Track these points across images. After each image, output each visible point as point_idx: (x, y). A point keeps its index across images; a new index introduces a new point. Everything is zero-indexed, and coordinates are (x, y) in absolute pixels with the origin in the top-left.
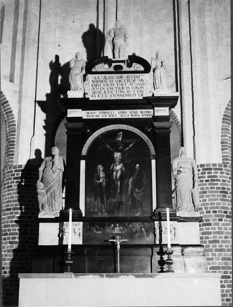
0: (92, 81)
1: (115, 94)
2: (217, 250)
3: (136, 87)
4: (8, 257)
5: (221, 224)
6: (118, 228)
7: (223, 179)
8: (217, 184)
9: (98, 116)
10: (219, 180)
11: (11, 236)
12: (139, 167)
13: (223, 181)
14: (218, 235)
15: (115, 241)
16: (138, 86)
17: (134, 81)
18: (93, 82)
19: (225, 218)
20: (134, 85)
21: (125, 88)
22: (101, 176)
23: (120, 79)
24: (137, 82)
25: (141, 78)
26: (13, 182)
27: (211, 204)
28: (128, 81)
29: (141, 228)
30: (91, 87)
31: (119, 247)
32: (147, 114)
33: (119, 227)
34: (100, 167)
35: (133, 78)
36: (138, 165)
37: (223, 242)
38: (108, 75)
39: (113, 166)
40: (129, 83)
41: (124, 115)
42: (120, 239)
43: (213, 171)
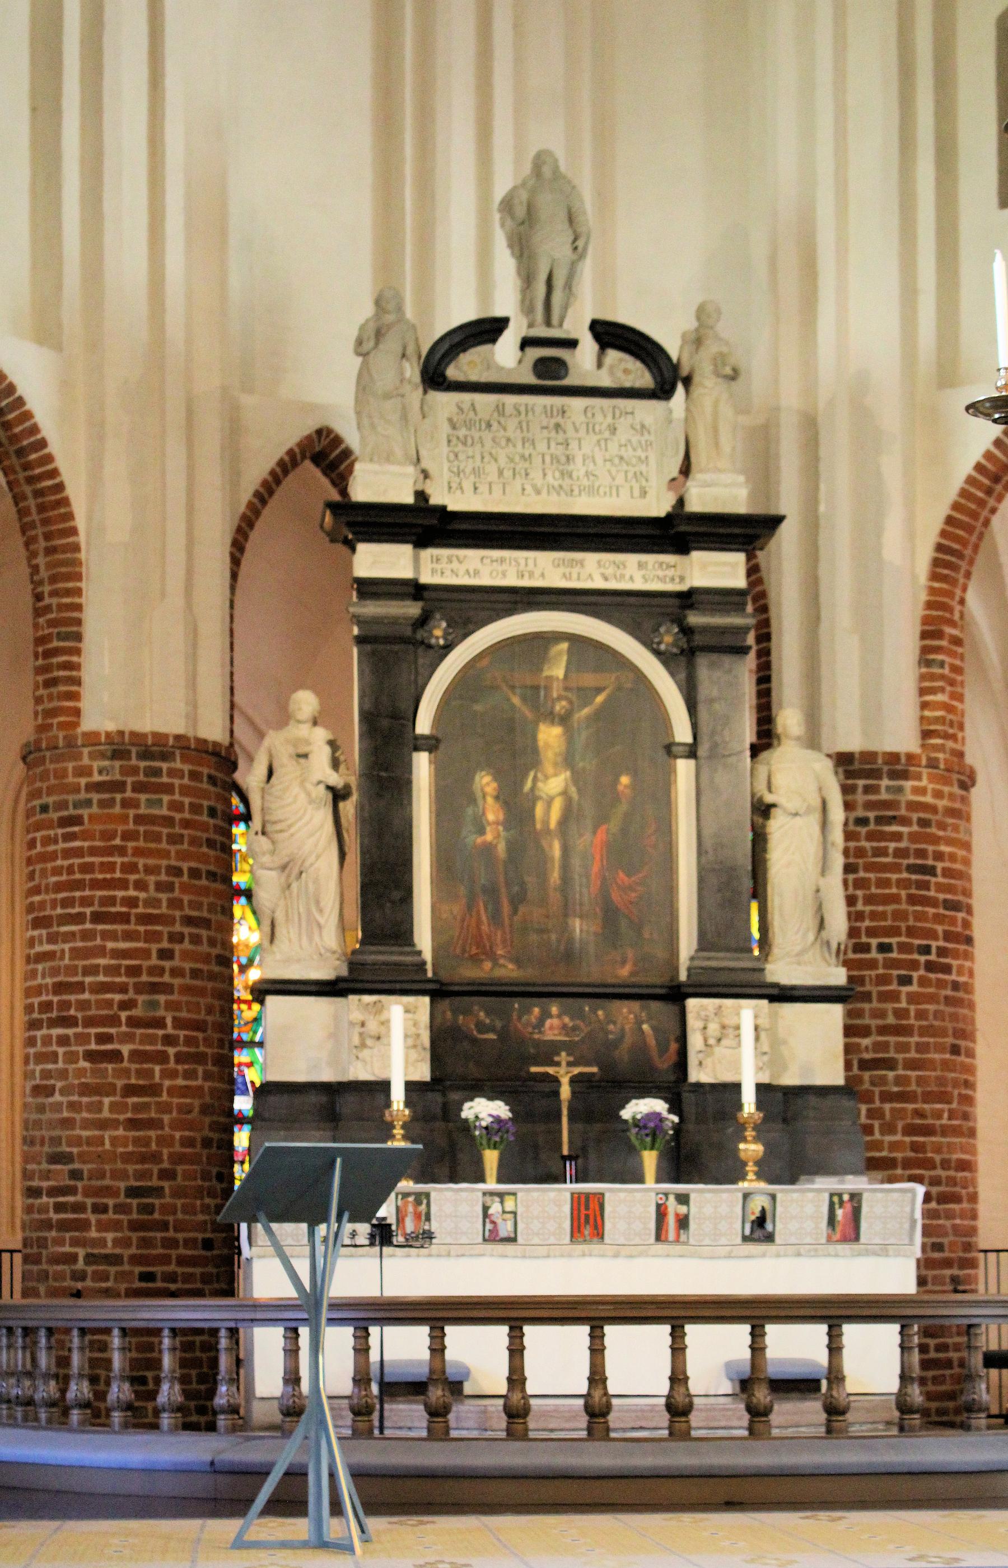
0: (450, 420)
1: (539, 482)
2: (887, 1097)
3: (621, 458)
4: (85, 1115)
5: (909, 994)
6: (555, 1022)
7: (922, 815)
8: (897, 837)
9: (477, 573)
10: (905, 821)
11: (93, 1031)
12: (633, 786)
13: (924, 823)
14: (892, 1039)
15: (551, 1070)
16: (628, 453)
17: (613, 430)
18: (454, 427)
19: (922, 972)
20: (613, 448)
21: (579, 460)
22: (491, 817)
23: (559, 419)
24: (624, 434)
25: (638, 419)
26: (88, 803)
27: (874, 916)
28: (590, 428)
29: (639, 1023)
30: (445, 449)
31: (565, 1092)
32: (660, 573)
33: (559, 1016)
34: (485, 782)
35: (609, 419)
36: (625, 780)
37: (912, 1065)
38: (510, 400)
39: (535, 779)
40: (596, 438)
41: (575, 571)
42: (569, 1064)
43: (885, 782)
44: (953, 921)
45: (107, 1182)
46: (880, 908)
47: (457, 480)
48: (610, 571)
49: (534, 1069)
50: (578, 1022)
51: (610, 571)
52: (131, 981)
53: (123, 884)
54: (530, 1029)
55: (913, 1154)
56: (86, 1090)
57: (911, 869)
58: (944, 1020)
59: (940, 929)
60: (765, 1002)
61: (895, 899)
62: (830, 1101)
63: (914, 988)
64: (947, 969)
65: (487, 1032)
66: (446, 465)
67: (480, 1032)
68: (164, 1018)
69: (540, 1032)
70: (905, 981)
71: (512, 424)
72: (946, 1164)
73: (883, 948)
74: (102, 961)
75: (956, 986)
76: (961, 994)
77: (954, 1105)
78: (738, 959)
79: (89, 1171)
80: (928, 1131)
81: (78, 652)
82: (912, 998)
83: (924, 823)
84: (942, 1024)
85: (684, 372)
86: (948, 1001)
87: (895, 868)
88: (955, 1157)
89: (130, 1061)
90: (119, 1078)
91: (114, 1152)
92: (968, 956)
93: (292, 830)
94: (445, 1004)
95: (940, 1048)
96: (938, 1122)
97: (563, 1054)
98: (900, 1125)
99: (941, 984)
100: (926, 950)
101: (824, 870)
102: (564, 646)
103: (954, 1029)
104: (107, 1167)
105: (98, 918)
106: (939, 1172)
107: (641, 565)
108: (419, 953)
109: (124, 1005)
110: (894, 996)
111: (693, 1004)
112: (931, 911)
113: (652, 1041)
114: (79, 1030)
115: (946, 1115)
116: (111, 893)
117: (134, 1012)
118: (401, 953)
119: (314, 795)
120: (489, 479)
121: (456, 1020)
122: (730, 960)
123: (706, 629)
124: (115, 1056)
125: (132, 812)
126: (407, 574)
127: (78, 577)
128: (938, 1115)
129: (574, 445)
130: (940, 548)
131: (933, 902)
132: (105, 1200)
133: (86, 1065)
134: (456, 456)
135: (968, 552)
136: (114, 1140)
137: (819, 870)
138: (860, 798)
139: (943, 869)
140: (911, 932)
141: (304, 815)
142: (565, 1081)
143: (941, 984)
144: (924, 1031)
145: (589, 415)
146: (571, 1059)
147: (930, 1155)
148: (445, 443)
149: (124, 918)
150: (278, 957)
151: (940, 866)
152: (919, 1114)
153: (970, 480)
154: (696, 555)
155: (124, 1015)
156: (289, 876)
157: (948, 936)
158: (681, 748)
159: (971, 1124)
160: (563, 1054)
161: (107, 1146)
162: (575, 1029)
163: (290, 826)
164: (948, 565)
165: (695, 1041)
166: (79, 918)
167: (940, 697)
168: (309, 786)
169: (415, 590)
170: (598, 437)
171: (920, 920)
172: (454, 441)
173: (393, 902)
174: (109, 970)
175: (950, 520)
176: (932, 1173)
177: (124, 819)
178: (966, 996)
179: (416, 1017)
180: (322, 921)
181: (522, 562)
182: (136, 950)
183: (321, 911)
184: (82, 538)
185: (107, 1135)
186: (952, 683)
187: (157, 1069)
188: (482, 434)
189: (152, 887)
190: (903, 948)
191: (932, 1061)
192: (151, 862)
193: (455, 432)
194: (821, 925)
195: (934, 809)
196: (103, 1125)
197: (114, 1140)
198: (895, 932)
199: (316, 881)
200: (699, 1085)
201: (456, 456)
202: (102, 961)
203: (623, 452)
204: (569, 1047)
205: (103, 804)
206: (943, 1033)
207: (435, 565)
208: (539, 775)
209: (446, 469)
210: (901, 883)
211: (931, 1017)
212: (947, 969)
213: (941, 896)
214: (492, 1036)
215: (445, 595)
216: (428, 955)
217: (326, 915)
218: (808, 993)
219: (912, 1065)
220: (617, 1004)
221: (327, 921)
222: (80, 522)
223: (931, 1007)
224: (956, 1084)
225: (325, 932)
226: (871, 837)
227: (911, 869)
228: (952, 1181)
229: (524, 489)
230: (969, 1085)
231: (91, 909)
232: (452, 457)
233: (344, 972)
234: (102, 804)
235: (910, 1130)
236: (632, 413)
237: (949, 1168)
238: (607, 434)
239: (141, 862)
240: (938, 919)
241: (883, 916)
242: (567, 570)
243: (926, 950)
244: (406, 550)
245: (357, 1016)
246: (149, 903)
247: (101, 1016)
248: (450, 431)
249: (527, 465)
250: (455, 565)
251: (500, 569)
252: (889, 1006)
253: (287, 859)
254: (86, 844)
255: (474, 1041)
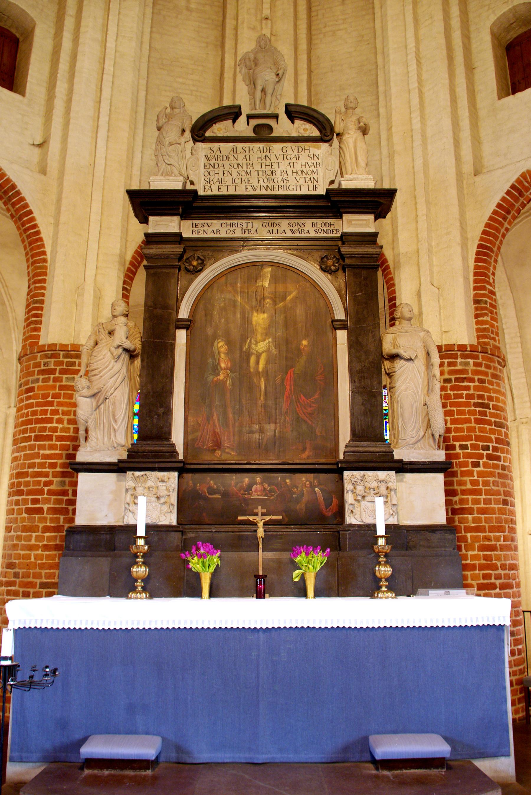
1: (255, 184)
3: (302, 171)
6: (259, 487)
7: (480, 377)
8: (467, 388)
10: (472, 380)
13: (481, 381)
15: (251, 518)
16: (306, 169)
17: (297, 158)
18: (208, 159)
19: (485, 460)
20: (298, 167)
21: (278, 173)
25: (311, 153)
27: (457, 430)
29: (312, 486)
35: (296, 152)
37: (482, 511)
38: (240, 146)
40: (287, 162)
42: (263, 514)
43: (459, 360)
44: (500, 433)
45: (31, 579)
46: (460, 426)
47: (209, 185)
48: (296, 228)
49: (240, 518)
50: (273, 487)
51: (296, 228)
52: (51, 471)
53: (50, 421)
54: (242, 492)
55: (485, 562)
56: (25, 529)
57: (476, 405)
58: (498, 486)
59: (493, 436)
60: (393, 473)
61: (468, 421)
62: (436, 537)
63: (481, 468)
64: (498, 458)
65: (215, 493)
66: (203, 178)
67: (210, 494)
68: (68, 490)
69: (249, 494)
70: (477, 465)
71: (241, 157)
72: (503, 567)
73: (462, 447)
74: (37, 461)
75: (504, 468)
76: (506, 472)
77: (506, 533)
78: (376, 446)
79: (23, 573)
80: (493, 548)
81: (42, 309)
82: (480, 474)
83: (481, 381)
84: (497, 488)
85: (337, 130)
86: (500, 476)
87: (468, 405)
88: (508, 562)
89: (47, 514)
90: (41, 522)
91: (36, 563)
92: (508, 452)
93: (101, 374)
94: (188, 476)
95: (497, 502)
96: (498, 543)
97: (260, 507)
98: (477, 545)
99: (496, 467)
100: (487, 448)
101: (429, 392)
102: (268, 270)
103: (504, 491)
104: (31, 571)
105: (37, 438)
106: (500, 571)
107: (313, 225)
108: (173, 445)
109: (46, 484)
110: (470, 473)
111: (346, 474)
112: (488, 427)
113: (321, 499)
114: (24, 497)
115: (502, 539)
116: (45, 425)
117: (52, 487)
118: (161, 445)
119: (115, 354)
120: (227, 184)
121: (195, 485)
122: (372, 446)
123: (351, 256)
124: (40, 511)
125: (58, 384)
126: (176, 230)
127: (45, 274)
128: (498, 539)
129: (276, 166)
130: (480, 246)
131: (489, 423)
132: (28, 590)
133: (26, 515)
134: (209, 173)
135: (495, 249)
136: (36, 557)
137: (426, 392)
138: (446, 369)
139: (493, 405)
140: (478, 438)
141: (109, 364)
142: (261, 524)
143: (496, 467)
144: (487, 493)
145: (284, 151)
146: (265, 511)
147: (494, 562)
148: (203, 166)
149: (50, 438)
150: (89, 449)
151: (491, 403)
152: (488, 539)
153: (495, 212)
154: (345, 217)
155: (46, 489)
156: (98, 401)
157: (498, 441)
158: (338, 323)
159: (515, 543)
160: (260, 507)
161: (33, 560)
162: (270, 491)
163: (100, 372)
164: (485, 254)
165: (349, 498)
166: (28, 439)
167: (485, 318)
168: (113, 349)
169: (177, 238)
170: (290, 161)
171: (482, 432)
172: (208, 166)
173: (159, 415)
174: (42, 465)
175: (484, 232)
176: (496, 572)
177: (54, 387)
178: (509, 473)
179: (168, 484)
180: (116, 427)
181: (245, 225)
182: (55, 454)
183: (116, 421)
184: (48, 257)
185: (33, 553)
186: (492, 312)
187: (62, 517)
188: (224, 162)
189: (65, 422)
190: (474, 447)
191: (493, 509)
192: (65, 409)
193: (209, 162)
194: (429, 425)
195: (486, 374)
196: (31, 548)
197: (36, 557)
198: (469, 438)
199: (114, 403)
200: (351, 525)
201: (209, 173)
202: (37, 461)
203: (303, 168)
204: (262, 502)
205: (44, 380)
206: (498, 493)
207: (194, 229)
208: (253, 341)
209: (203, 180)
210: (470, 413)
211: (491, 485)
212: (498, 458)
213: (493, 420)
214: (218, 496)
215: (199, 244)
216: (180, 449)
217: (119, 424)
218: (423, 467)
219: (482, 511)
220: (298, 475)
221: (119, 427)
222: (48, 249)
223: (491, 479)
224: (506, 522)
225: (118, 434)
226: (452, 388)
227: (476, 405)
228: (507, 577)
229: (246, 188)
230: (513, 522)
231: (35, 434)
232: (206, 174)
233: (124, 456)
234: (44, 380)
235: (482, 548)
236: (334, 225)
237: (505, 569)
238: (294, 160)
239: (61, 409)
240: (492, 431)
241: (462, 430)
242: (271, 229)
243: (487, 448)
244: (176, 219)
245: (131, 484)
246: (63, 430)
247: (35, 489)
248: (206, 161)
249: (249, 176)
250: (206, 228)
251: (232, 229)
252: (467, 479)
253: (96, 391)
254: (35, 401)
255: (207, 499)
